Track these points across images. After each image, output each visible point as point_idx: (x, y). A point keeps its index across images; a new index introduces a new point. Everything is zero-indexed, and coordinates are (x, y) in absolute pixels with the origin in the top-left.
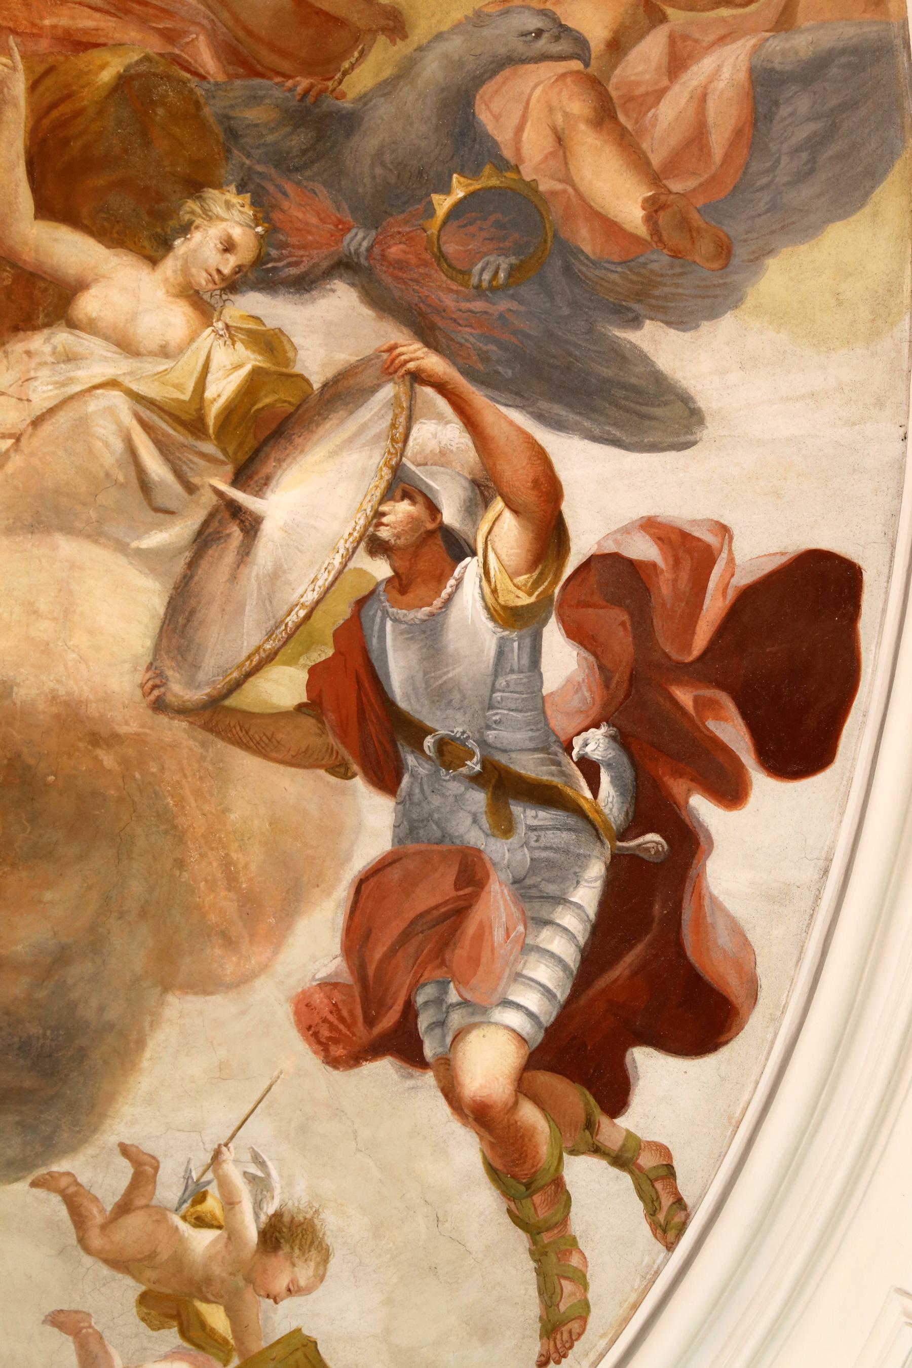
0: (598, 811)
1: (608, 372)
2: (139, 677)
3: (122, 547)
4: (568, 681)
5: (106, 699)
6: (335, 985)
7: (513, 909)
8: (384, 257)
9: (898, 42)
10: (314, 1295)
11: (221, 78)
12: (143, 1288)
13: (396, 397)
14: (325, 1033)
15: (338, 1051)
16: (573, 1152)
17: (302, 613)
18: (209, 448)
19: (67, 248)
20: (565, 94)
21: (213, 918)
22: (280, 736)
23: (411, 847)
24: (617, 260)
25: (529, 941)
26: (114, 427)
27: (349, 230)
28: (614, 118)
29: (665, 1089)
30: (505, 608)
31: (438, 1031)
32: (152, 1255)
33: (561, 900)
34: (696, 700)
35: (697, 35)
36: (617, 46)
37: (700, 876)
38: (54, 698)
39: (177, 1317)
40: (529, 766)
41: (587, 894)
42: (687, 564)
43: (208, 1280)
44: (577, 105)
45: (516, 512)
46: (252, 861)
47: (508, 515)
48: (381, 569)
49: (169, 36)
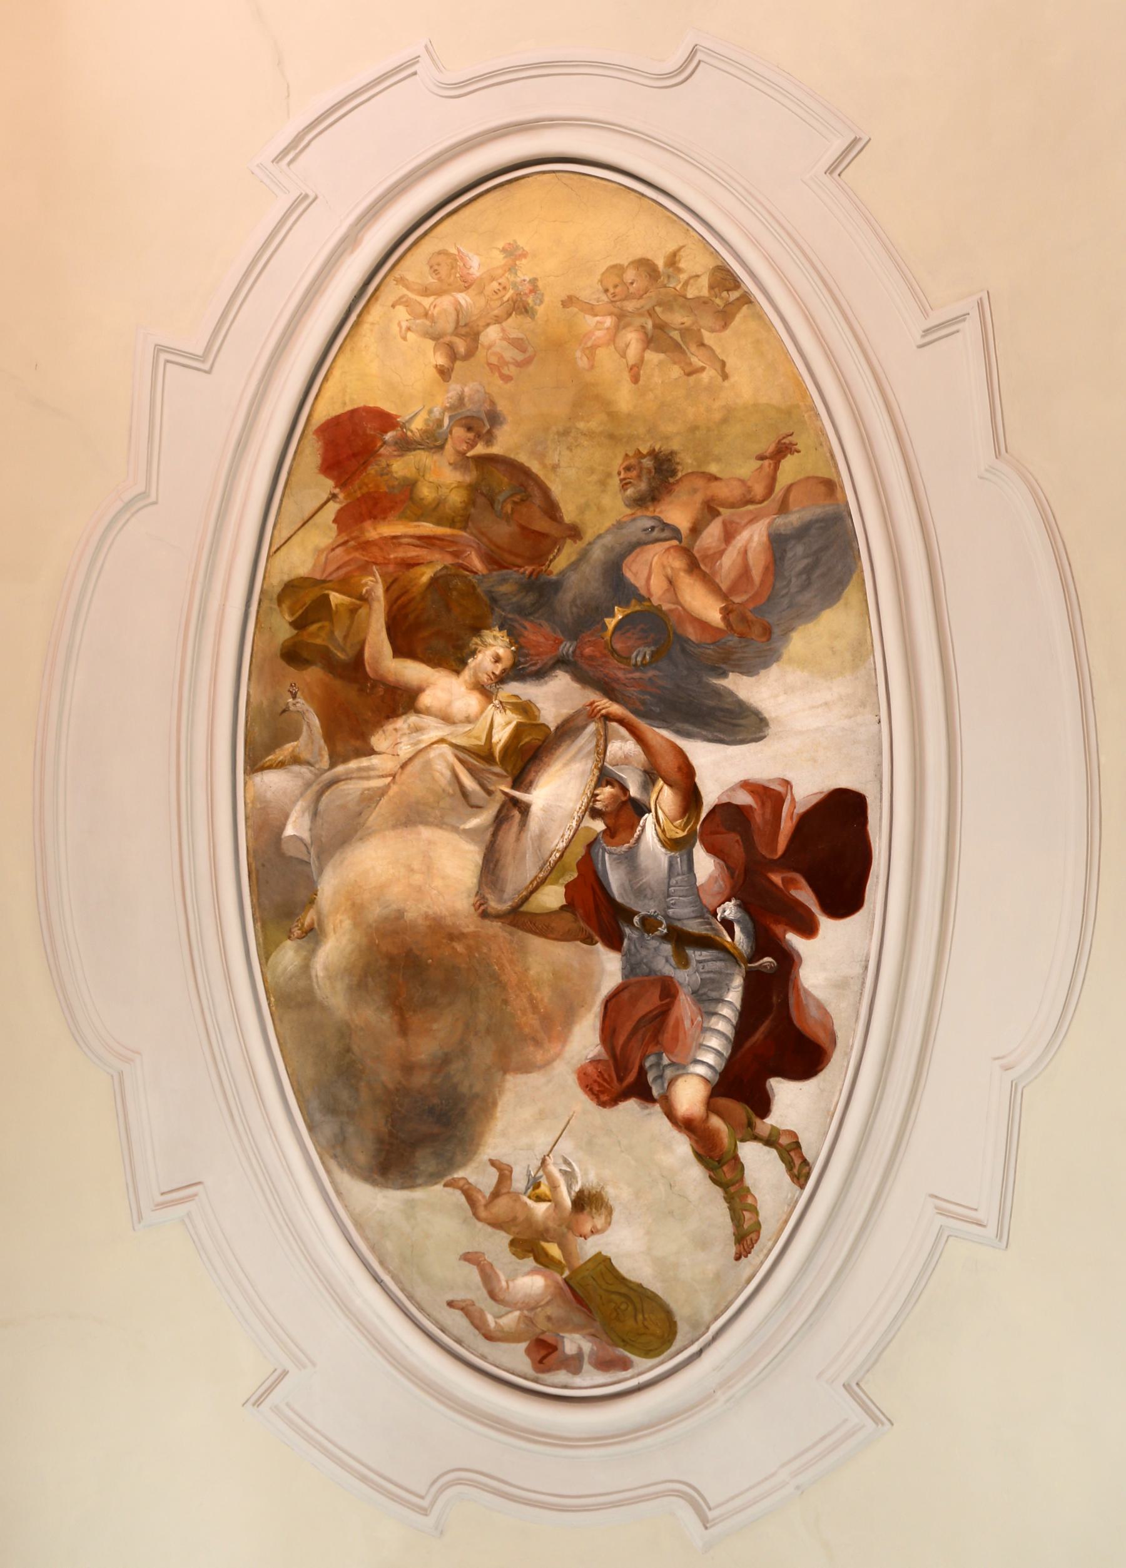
0: (736, 948)
1: (711, 703)
2: (472, 900)
3: (455, 829)
4: (710, 876)
5: (455, 914)
6: (599, 1061)
7: (694, 1008)
8: (582, 655)
9: (845, 513)
10: (606, 1233)
11: (485, 572)
12: (511, 1237)
13: (597, 730)
14: (596, 1088)
15: (604, 1098)
16: (743, 1140)
17: (558, 855)
18: (497, 769)
19: (412, 671)
20: (671, 559)
21: (527, 1030)
22: (553, 925)
23: (633, 979)
24: (709, 641)
25: (705, 1025)
26: (444, 764)
27: (561, 642)
28: (699, 567)
29: (791, 1101)
30: (671, 840)
31: (659, 1081)
32: (514, 1219)
33: (720, 1000)
34: (783, 880)
35: (738, 520)
36: (696, 530)
37: (797, 978)
38: (426, 917)
39: (532, 1251)
40: (694, 927)
41: (734, 995)
42: (769, 805)
43: (547, 1230)
44: (678, 563)
45: (670, 785)
46: (545, 996)
47: (666, 788)
48: (599, 826)
49: (456, 554)
